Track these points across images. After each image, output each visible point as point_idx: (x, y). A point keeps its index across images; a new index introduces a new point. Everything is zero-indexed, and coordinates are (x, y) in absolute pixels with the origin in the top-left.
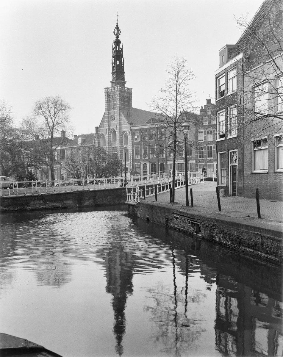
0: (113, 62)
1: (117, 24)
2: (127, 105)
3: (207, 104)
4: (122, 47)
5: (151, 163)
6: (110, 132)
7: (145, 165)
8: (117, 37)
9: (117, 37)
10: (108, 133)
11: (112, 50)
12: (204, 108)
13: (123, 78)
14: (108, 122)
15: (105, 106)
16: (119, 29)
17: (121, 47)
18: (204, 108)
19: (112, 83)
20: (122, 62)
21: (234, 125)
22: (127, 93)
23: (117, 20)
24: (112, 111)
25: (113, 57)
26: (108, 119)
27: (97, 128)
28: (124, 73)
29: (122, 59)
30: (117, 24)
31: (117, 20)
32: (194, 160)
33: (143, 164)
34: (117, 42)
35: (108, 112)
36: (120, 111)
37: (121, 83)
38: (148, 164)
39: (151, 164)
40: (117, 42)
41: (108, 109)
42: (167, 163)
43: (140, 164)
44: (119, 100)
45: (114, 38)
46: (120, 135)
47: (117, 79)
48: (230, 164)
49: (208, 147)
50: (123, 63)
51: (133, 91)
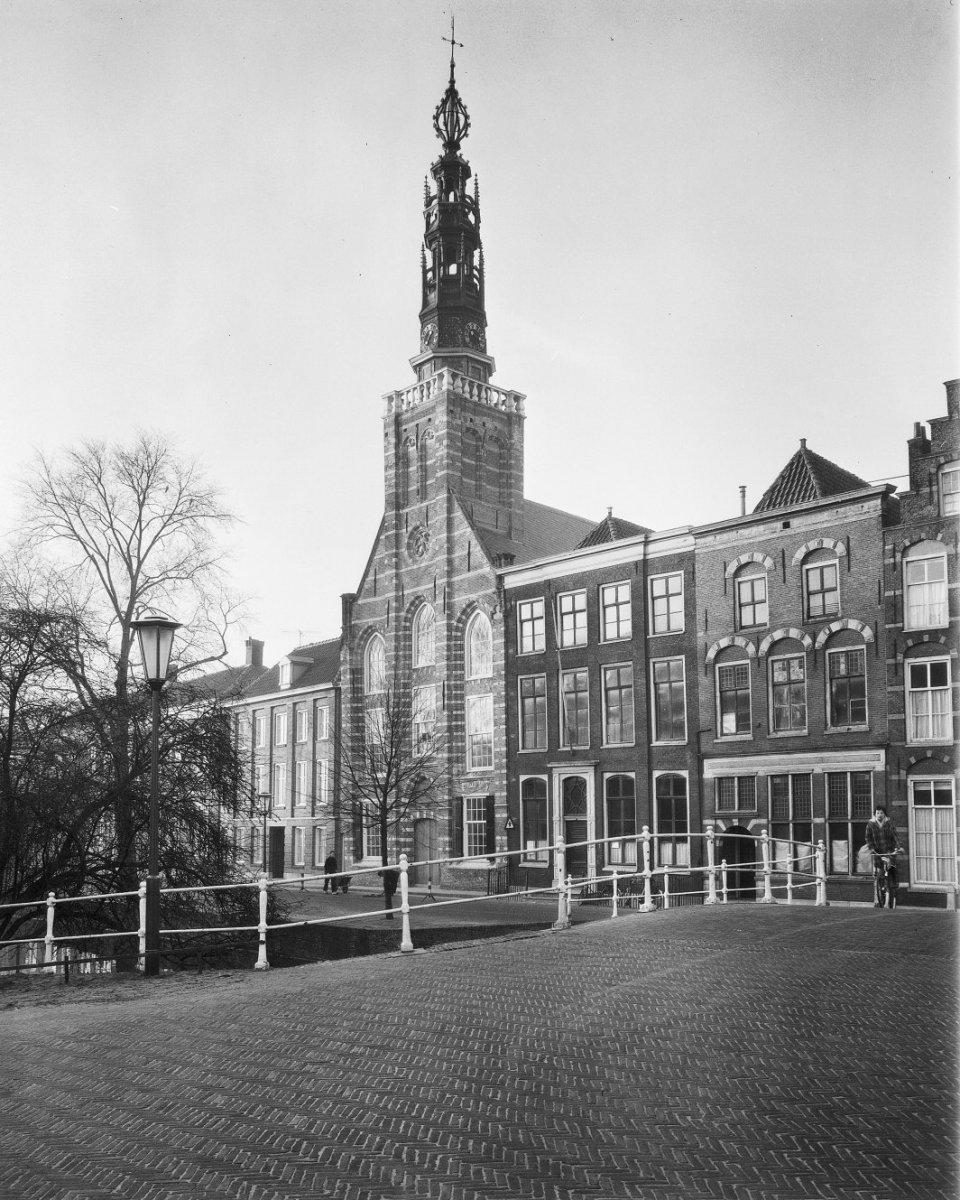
0: (429, 264)
1: (452, 82)
2: (834, 809)
3: (911, 489)
4: (477, 192)
5: (607, 775)
6: (403, 614)
7: (574, 790)
8: (452, 145)
9: (452, 145)
10: (397, 618)
11: (424, 209)
12: (929, 437)
13: (478, 342)
14: (397, 566)
15: (382, 484)
16: (461, 105)
17: (469, 190)
18: (929, 437)
19: (418, 368)
20: (476, 262)
21: (297, 1029)
22: (491, 412)
23: (453, 66)
24: (413, 509)
25: (429, 238)
26: (397, 548)
27: (349, 601)
28: (480, 318)
29: (476, 253)
30: (452, 82)
31: (453, 66)
32: (882, 753)
33: (565, 781)
34: (452, 171)
35: (398, 517)
36: (449, 500)
37: (464, 363)
38: (589, 777)
39: (610, 781)
40: (452, 171)
41: (397, 501)
42: (700, 771)
43: (545, 777)
44: (445, 442)
45: (436, 150)
46: (449, 627)
47: (442, 343)
48: (657, 740)
49: (859, 715)
50: (481, 271)
51: (528, 408)
